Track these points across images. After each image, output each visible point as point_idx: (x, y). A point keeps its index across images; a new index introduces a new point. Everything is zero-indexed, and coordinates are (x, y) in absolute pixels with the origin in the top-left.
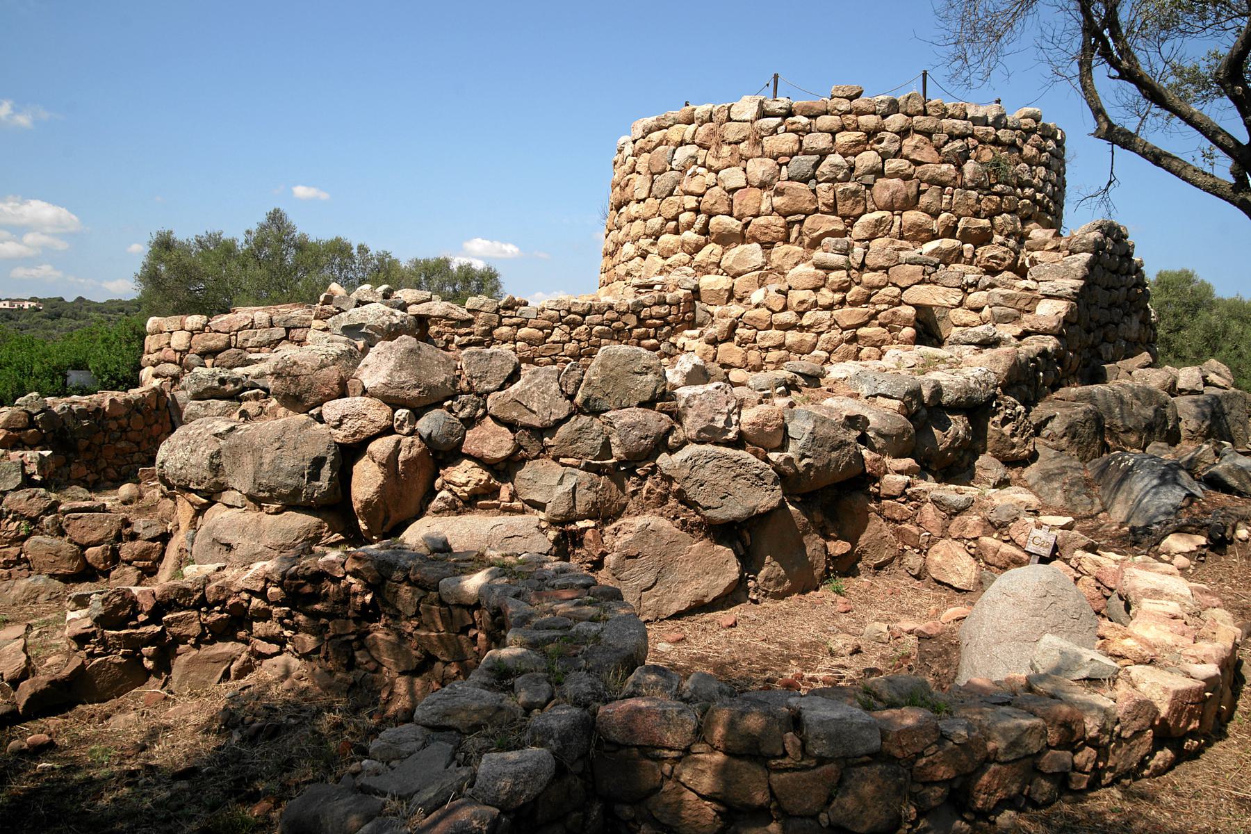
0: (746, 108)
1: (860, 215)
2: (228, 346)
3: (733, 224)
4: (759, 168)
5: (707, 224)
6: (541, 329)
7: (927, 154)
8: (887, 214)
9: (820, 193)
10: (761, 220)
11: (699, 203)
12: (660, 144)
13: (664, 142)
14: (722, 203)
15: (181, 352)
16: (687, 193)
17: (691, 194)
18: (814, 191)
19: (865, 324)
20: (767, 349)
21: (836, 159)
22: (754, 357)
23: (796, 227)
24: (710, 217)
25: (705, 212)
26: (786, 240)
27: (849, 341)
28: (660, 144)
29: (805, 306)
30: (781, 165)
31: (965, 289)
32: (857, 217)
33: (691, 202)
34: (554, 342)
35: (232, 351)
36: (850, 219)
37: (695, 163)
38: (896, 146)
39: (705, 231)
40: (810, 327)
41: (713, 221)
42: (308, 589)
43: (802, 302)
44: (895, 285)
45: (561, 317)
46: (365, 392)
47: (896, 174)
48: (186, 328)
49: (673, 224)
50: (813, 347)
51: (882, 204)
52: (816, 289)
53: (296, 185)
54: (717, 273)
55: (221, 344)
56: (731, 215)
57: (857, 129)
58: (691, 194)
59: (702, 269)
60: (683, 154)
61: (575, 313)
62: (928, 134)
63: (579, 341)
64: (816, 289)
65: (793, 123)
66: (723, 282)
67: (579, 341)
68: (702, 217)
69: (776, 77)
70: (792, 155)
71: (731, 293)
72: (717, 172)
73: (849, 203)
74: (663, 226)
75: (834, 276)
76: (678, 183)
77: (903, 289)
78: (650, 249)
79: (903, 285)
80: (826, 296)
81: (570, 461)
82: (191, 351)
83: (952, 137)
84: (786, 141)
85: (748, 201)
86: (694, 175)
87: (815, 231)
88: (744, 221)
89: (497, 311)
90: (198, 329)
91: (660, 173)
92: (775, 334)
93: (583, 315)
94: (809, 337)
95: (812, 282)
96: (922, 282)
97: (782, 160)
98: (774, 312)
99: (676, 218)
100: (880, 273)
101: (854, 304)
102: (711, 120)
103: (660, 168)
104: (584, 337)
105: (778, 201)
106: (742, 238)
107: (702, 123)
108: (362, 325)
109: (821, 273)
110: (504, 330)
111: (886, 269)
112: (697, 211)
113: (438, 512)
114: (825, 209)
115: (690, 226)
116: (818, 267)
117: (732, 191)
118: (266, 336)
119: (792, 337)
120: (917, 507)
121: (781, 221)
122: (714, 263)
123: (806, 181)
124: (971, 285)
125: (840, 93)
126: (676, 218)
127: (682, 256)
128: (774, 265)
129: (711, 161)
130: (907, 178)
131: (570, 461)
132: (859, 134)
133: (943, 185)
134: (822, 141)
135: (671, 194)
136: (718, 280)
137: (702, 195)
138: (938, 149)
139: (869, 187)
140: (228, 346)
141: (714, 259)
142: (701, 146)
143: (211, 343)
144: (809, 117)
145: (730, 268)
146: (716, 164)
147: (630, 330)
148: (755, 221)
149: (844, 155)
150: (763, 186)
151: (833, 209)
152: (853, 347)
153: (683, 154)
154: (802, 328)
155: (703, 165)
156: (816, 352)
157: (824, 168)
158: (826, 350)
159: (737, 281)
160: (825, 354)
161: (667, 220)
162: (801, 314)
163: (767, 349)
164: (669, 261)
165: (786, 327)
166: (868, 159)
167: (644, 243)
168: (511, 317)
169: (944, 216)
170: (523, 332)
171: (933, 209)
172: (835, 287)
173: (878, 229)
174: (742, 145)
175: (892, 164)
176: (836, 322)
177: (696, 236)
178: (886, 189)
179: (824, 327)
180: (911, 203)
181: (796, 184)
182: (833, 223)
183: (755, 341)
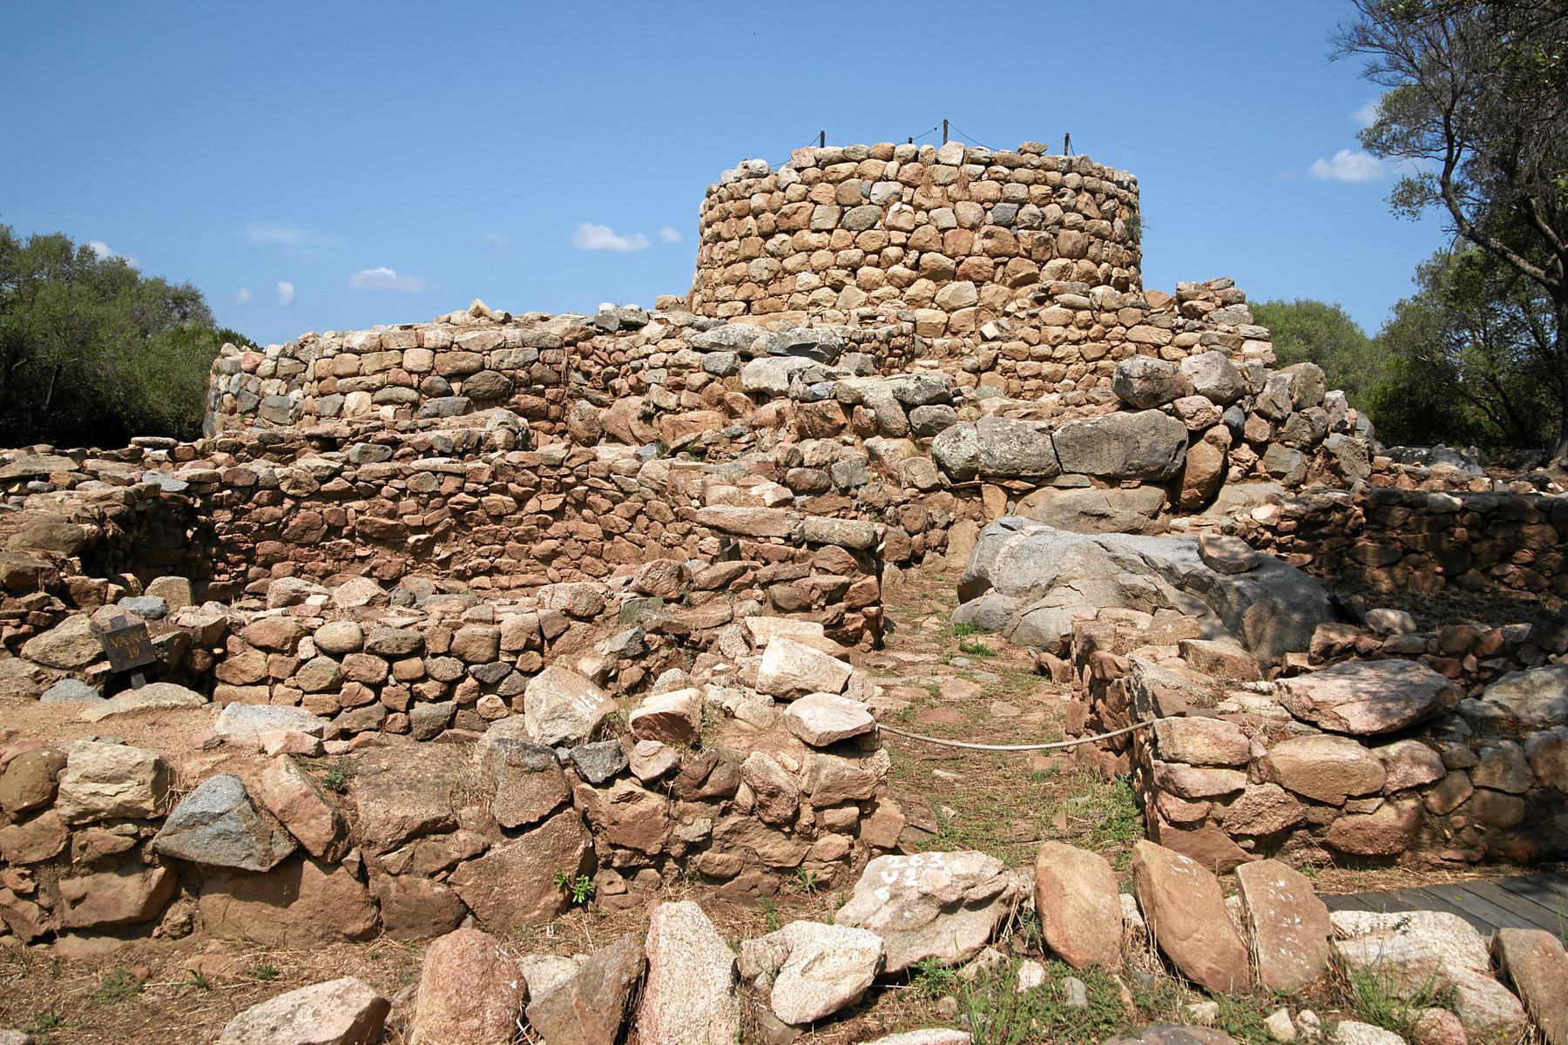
0: (952, 152)
2: (482, 368)
4: (970, 212)
7: (1092, 211)
8: (1069, 261)
9: (1022, 239)
11: (908, 239)
12: (851, 176)
14: (937, 242)
15: (419, 373)
16: (891, 228)
17: (900, 229)
18: (1015, 236)
20: (1026, 378)
23: (1001, 268)
24: (921, 254)
25: (916, 248)
27: (1093, 372)
28: (851, 176)
31: (1174, 330)
32: (1045, 262)
33: (898, 237)
35: (485, 373)
36: (1041, 263)
37: (900, 199)
39: (916, 266)
40: (1062, 359)
42: (1322, 517)
43: (1056, 337)
44: (1122, 325)
46: (1196, 392)
47: (1074, 227)
48: (426, 344)
50: (1064, 377)
52: (1066, 326)
54: (931, 307)
55: (474, 365)
57: (1045, 183)
58: (900, 229)
59: (914, 302)
60: (880, 191)
62: (1093, 192)
64: (1066, 326)
66: (940, 317)
69: (946, 122)
70: (995, 202)
71: (947, 326)
72: (928, 211)
73: (1041, 249)
76: (880, 217)
77: (1128, 328)
78: (847, 280)
80: (1074, 333)
81: (1291, 443)
82: (434, 372)
83: (1110, 197)
84: (989, 188)
88: (957, 259)
90: (445, 347)
91: (853, 206)
94: (1061, 367)
95: (1064, 320)
98: (1031, 345)
99: (878, 252)
100: (1113, 314)
101: (1095, 340)
102: (915, 159)
103: (854, 201)
105: (988, 243)
106: (953, 276)
107: (906, 162)
108: (813, 345)
111: (1116, 310)
113: (1235, 481)
114: (1024, 253)
115: (898, 260)
117: (944, 230)
118: (521, 357)
119: (1047, 367)
120: (1396, 478)
121: (991, 262)
123: (1009, 227)
124: (1180, 327)
125: (1031, 149)
129: (919, 199)
130: (1082, 230)
131: (1291, 443)
134: (1020, 191)
135: (872, 227)
138: (1099, 206)
140: (482, 368)
141: (930, 294)
142: (906, 184)
143: (463, 364)
144: (1009, 168)
145: (946, 303)
146: (927, 203)
149: (1039, 206)
150: (974, 228)
151: (1029, 254)
152: (1094, 377)
153: (880, 191)
154: (1055, 360)
155: (910, 203)
156: (1065, 382)
158: (1074, 379)
159: (954, 315)
160: (1073, 383)
162: (1054, 347)
163: (1026, 378)
164: (875, 293)
165: (1042, 359)
166: (1053, 211)
169: (1105, 265)
172: (1081, 325)
174: (950, 188)
176: (1082, 355)
177: (908, 271)
178: (1069, 238)
180: (1083, 254)
181: (1002, 229)
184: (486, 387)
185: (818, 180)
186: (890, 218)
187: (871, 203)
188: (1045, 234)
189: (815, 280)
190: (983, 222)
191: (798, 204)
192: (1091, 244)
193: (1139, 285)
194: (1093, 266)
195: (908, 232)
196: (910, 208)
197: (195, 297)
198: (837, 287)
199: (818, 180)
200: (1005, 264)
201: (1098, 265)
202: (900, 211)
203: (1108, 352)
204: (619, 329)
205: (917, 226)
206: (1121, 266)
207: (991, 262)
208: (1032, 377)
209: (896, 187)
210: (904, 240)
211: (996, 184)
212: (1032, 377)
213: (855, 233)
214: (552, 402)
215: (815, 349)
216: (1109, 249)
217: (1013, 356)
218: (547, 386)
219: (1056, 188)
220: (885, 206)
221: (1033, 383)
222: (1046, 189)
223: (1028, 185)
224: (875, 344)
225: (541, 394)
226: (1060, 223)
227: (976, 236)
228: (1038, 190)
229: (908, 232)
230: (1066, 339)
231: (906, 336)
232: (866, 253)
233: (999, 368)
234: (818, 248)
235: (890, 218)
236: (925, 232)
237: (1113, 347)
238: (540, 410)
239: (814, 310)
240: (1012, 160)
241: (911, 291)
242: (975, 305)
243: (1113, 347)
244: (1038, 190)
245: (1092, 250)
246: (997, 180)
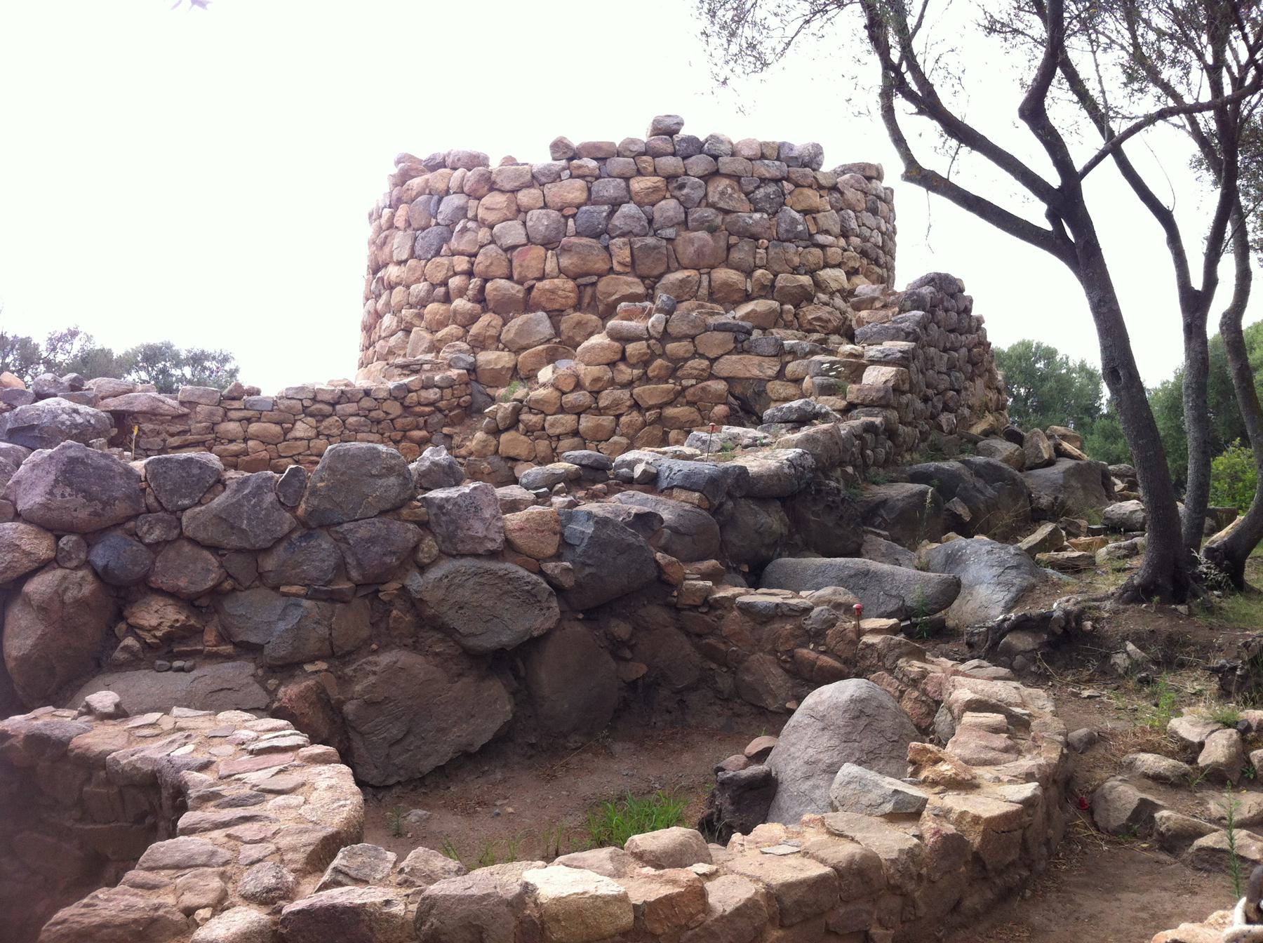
3: (515, 290)
5: (482, 289)
10: (546, 284)
13: (427, 192)
20: (558, 437)
23: (589, 290)
24: (486, 281)
29: (600, 385)
30: (566, 218)
33: (461, 263)
37: (465, 216)
41: (489, 285)
44: (702, 356)
49: (442, 289)
59: (479, 344)
68: (476, 282)
72: (491, 227)
74: (430, 292)
75: (631, 348)
79: (712, 356)
80: (626, 373)
85: (533, 259)
86: (465, 230)
87: (611, 295)
88: (526, 285)
92: (568, 420)
93: (333, 405)
94: (607, 421)
97: (568, 211)
105: (565, 261)
112: (470, 274)
119: (586, 422)
121: (570, 284)
123: (597, 236)
135: (437, 253)
136: (499, 358)
137: (475, 255)
141: (492, 332)
145: (512, 341)
146: (491, 217)
148: (539, 285)
149: (640, 205)
154: (600, 411)
155: (475, 219)
161: (434, 286)
164: (439, 335)
165: (579, 412)
170: (254, 427)
183: (543, 429)
186: (454, 244)
200: (594, 284)
211: (580, 183)
213: (423, 262)
219: (670, 178)
232: (434, 286)
233: (521, 426)
243: (684, 389)
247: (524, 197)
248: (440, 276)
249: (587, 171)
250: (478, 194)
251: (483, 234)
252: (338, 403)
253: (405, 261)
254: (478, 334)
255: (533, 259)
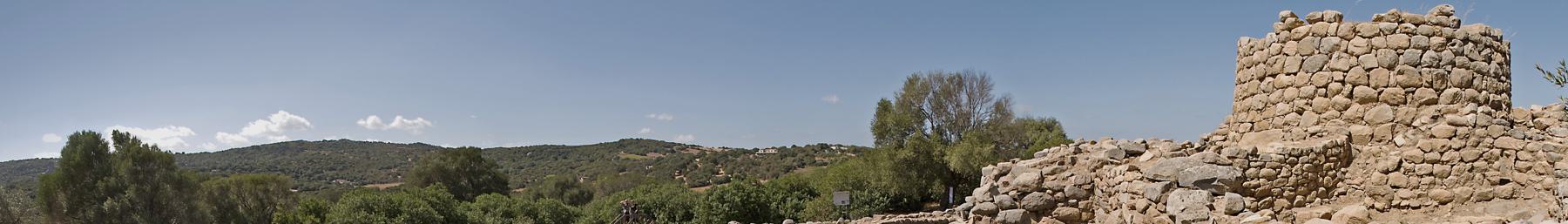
1: (1444, 89)
3: (1372, 93)
6: (1275, 169)
8: (1459, 89)
11: (1345, 77)
12: (1307, 34)
13: (1311, 34)
16: (1332, 70)
18: (1420, 73)
19: (1476, 160)
20: (1422, 176)
21: (1430, 53)
22: (1414, 180)
24: (1354, 87)
26: (1405, 103)
27: (1470, 171)
28: (1307, 34)
29: (1445, 149)
30: (1399, 55)
32: (1443, 91)
33: (1339, 76)
34: (1282, 177)
36: (1439, 92)
38: (1461, 49)
40: (1448, 162)
43: (1443, 147)
45: (1286, 159)
51: (1456, 84)
52: (1450, 138)
53: (359, 119)
56: (1368, 85)
57: (1441, 36)
59: (1352, 121)
61: (1293, 156)
63: (1297, 175)
65: (1406, 28)
66: (1367, 130)
67: (1297, 175)
72: (1358, 57)
73: (1439, 81)
74: (1316, 92)
75: (1461, 130)
76: (1326, 62)
77: (1495, 139)
80: (1456, 143)
85: (1380, 76)
86: (1339, 58)
87: (1423, 98)
88: (1379, 90)
89: (1247, 158)
93: (1298, 157)
94: (1447, 167)
96: (1503, 135)
97: (1400, 51)
98: (1425, 152)
99: (1326, 87)
100: (1484, 129)
103: (1309, 52)
104: (1300, 172)
105: (1400, 78)
108: (1215, 179)
109: (1453, 128)
110: (1252, 170)
114: (1427, 85)
115: (1338, 92)
116: (1450, 124)
119: (1437, 168)
121: (1403, 91)
122: (1359, 117)
126: (1326, 87)
127: (1333, 112)
128: (1399, 119)
132: (1442, 38)
133: (1483, 74)
134: (1423, 41)
135: (1321, 70)
137: (1347, 72)
139: (1449, 72)
145: (1372, 121)
146: (1357, 51)
147: (1322, 165)
148: (1385, 90)
151: (1431, 85)
155: (1346, 52)
157: (1426, 57)
162: (1442, 154)
163: (1422, 176)
164: (1323, 115)
165: (1433, 162)
166: (1447, 54)
167: (1301, 103)
168: (1256, 161)
169: (1484, 92)
170: (1264, 171)
171: (1479, 88)
173: (1455, 98)
175: (1459, 60)
178: (1458, 75)
179: (1456, 162)
180: (1470, 84)
182: (1429, 94)
183: (1414, 171)
184: (1034, 204)
185: (1288, 39)
187: (1319, 53)
188: (1441, 71)
189: (1287, 108)
190: (1397, 62)
191: (1276, 57)
192: (1474, 78)
193: (1509, 105)
194: (1476, 93)
195: (1344, 72)
196: (1345, 55)
197: (1054, 122)
198: (1300, 113)
199: (1288, 39)
201: (1480, 92)
202: (1339, 58)
203: (1481, 156)
204: (1126, 157)
205: (1351, 68)
206: (1496, 93)
207: (1403, 91)
208: (1427, 175)
209: (1336, 40)
210: (1342, 78)
212: (1427, 175)
214: (1083, 210)
215: (1215, 183)
216: (1488, 81)
217: (1411, 160)
218: (1079, 200)
219: (1449, 39)
220: (1330, 54)
221: (1427, 179)
222: (1441, 40)
223: (1429, 38)
224: (1312, 156)
225: (1076, 205)
226: (1453, 64)
227: (1392, 73)
228: (1436, 40)
229: (1344, 72)
230: (1450, 148)
231: (1340, 146)
233: (1402, 170)
234: (1288, 86)
235: (1333, 63)
236: (1355, 72)
237: (1484, 153)
238: (1074, 216)
239: (1286, 128)
240: (1417, 19)
241: (1347, 113)
242: (1392, 121)
244: (1436, 40)
245: (1476, 82)
246: (1407, 33)
247: (1376, 41)
248: (1324, 82)
249: (1410, 31)
250: (1348, 38)
251: (1353, 60)
252: (1300, 156)
253: (1295, 74)
254: (896, 103)
255: (1380, 76)
